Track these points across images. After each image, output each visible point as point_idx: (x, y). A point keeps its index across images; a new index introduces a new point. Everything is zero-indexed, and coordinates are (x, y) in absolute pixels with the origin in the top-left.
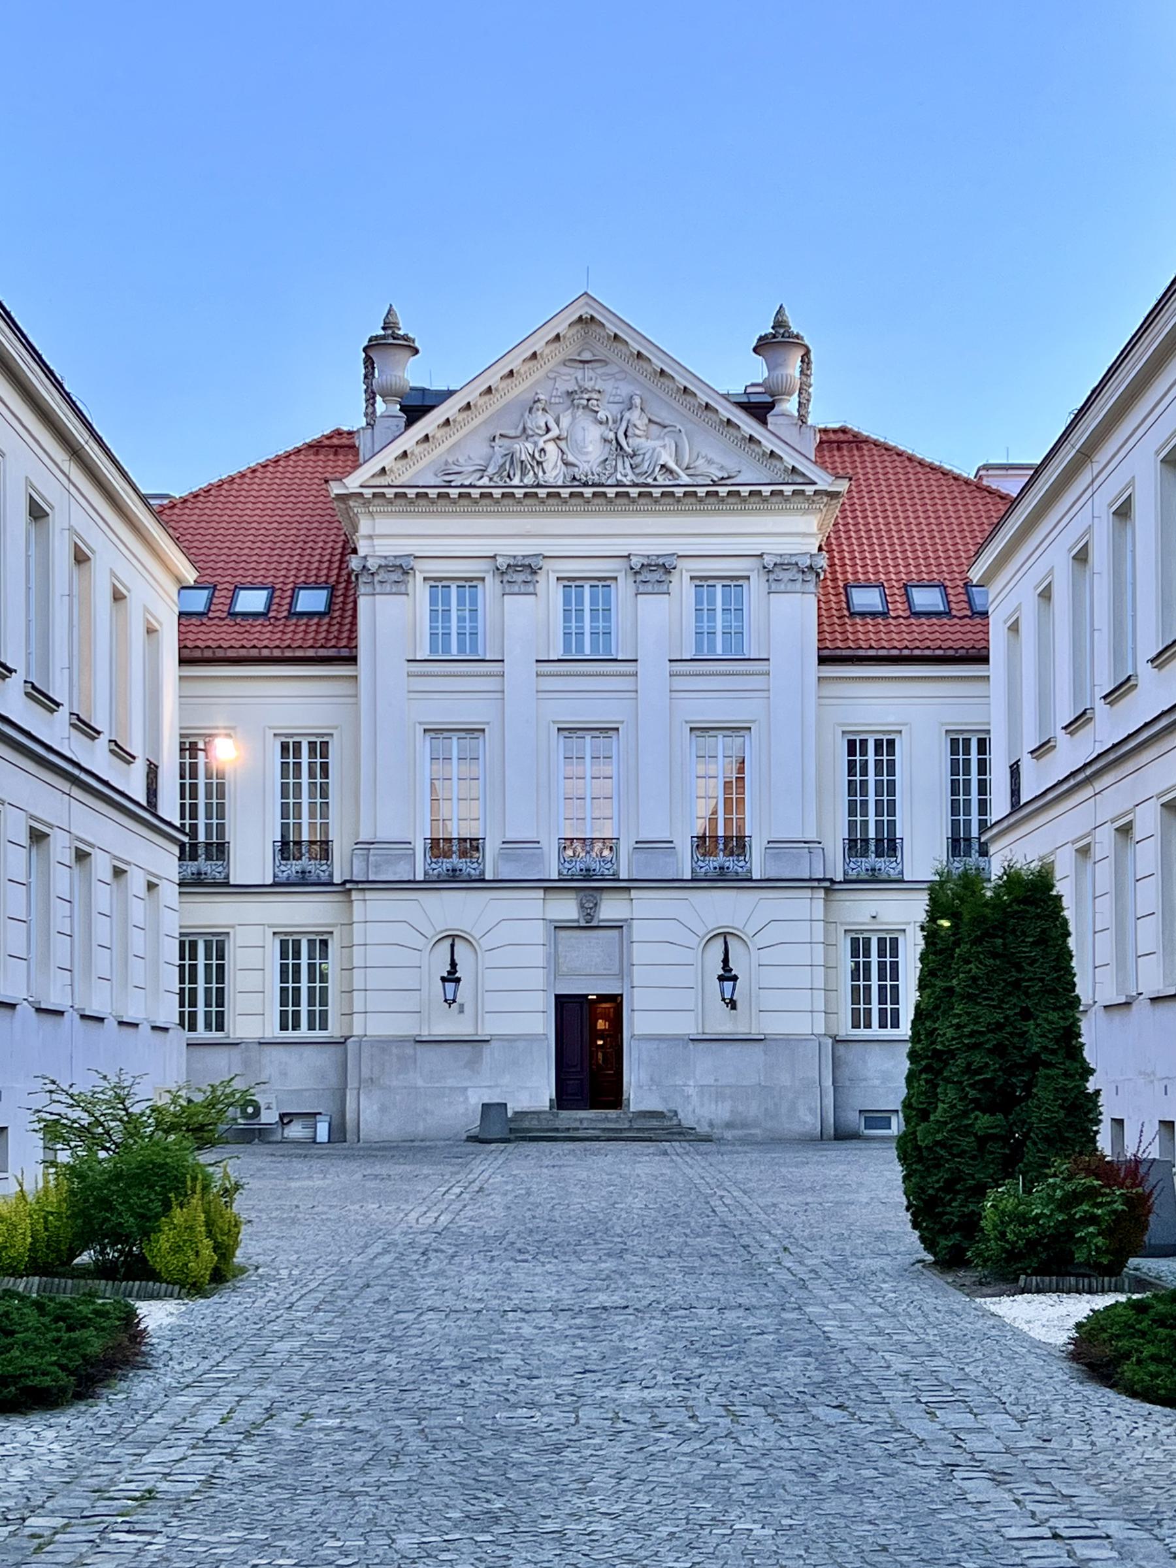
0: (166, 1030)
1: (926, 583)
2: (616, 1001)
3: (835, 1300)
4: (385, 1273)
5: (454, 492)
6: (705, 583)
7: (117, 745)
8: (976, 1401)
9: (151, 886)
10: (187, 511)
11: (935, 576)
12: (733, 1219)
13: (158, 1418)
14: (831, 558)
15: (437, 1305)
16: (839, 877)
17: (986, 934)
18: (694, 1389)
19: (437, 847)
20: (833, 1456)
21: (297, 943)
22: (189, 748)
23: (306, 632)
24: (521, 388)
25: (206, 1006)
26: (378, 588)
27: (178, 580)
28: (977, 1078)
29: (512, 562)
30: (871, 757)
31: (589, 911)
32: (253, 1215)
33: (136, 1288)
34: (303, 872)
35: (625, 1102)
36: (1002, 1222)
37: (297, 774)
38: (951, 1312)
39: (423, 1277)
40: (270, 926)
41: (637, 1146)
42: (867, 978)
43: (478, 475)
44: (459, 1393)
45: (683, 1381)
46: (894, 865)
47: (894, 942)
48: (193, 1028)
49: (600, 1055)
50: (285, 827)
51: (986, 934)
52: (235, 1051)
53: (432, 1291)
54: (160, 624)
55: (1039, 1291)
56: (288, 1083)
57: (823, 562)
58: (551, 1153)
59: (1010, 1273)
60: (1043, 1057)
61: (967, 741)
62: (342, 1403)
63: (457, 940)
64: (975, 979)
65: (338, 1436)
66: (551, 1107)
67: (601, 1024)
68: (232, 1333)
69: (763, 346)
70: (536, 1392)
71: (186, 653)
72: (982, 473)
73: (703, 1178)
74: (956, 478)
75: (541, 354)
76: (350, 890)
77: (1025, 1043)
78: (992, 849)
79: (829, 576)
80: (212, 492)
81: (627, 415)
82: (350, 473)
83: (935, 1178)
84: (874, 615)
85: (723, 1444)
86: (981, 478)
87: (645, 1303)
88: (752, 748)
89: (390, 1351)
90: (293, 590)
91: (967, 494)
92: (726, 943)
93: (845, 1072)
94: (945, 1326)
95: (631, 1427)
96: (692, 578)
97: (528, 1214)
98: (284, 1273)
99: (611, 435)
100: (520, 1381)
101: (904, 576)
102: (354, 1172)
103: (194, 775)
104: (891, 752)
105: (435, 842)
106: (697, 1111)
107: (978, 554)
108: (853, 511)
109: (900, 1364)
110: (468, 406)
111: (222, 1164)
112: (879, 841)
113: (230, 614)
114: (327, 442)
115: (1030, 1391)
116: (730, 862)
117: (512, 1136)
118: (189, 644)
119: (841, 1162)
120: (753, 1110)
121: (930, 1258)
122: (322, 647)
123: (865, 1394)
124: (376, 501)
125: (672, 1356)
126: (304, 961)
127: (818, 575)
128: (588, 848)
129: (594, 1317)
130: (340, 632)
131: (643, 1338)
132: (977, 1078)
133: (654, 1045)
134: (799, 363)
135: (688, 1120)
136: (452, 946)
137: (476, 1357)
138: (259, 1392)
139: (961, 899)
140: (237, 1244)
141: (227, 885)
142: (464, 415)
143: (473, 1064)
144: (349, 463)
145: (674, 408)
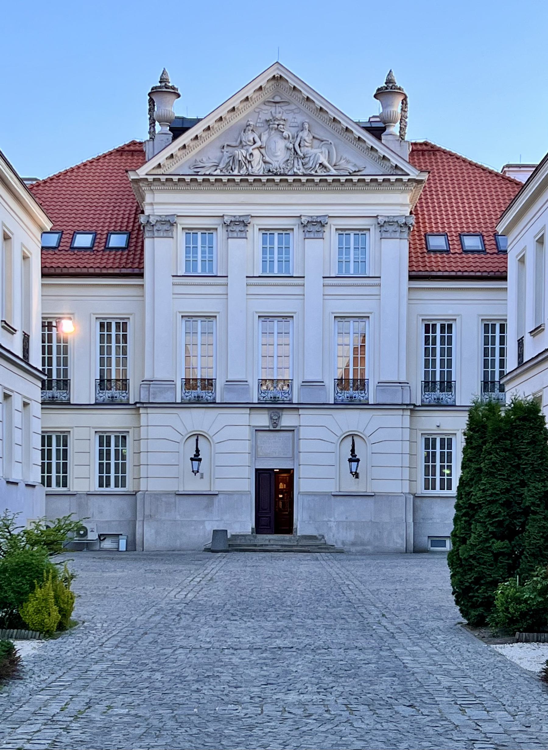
0: (34, 486)
1: (472, 233)
2: (290, 472)
3: (411, 645)
4: (156, 626)
5: (200, 179)
6: (344, 233)
7: (6, 323)
8: (489, 704)
9: (25, 404)
10: (46, 188)
11: (478, 230)
12: (354, 598)
13: (25, 708)
14: (417, 219)
15: (185, 645)
16: (419, 403)
17: (501, 438)
18: (329, 694)
19: (189, 384)
20: (406, 734)
21: (109, 438)
22: (47, 325)
23: (114, 259)
24: (239, 118)
25: (57, 473)
26: (156, 234)
27: (41, 228)
28: (494, 520)
29: (233, 219)
30: (438, 334)
31: (275, 422)
32: (82, 593)
33: (15, 633)
34: (112, 397)
35: (294, 530)
36: (507, 602)
37: (109, 341)
38: (477, 653)
39: (177, 628)
40: (94, 428)
41: (300, 555)
42: (434, 461)
43: (214, 168)
44: (195, 695)
45: (323, 690)
46: (450, 396)
47: (450, 440)
48: (49, 485)
49: (281, 503)
50: (102, 371)
51: (501, 438)
52: (73, 498)
53: (182, 637)
54: (31, 254)
55: (527, 641)
56: (103, 516)
57: (412, 220)
58: (252, 559)
59: (510, 631)
60: (532, 508)
61: (494, 326)
62: (130, 700)
63: (199, 437)
64: (494, 463)
65: (126, 719)
66: (252, 533)
67: (282, 486)
68: (68, 659)
69: (380, 94)
70: (239, 695)
71: (46, 271)
72: (505, 169)
73: (337, 574)
74: (490, 172)
75: (251, 98)
76: (139, 407)
77: (522, 500)
78: (506, 389)
79: (415, 229)
80: (61, 177)
81: (301, 134)
82: (140, 167)
83: (468, 577)
84: (441, 252)
85: (343, 726)
86: (505, 172)
87: (302, 645)
88: (370, 328)
89: (158, 671)
90: (107, 234)
91: (496, 182)
92: (353, 440)
93: (420, 514)
94: (472, 661)
95: (292, 716)
96: (260, 229)
97: (238, 593)
98: (99, 625)
99: (291, 146)
100: (230, 689)
101: (459, 229)
102: (140, 568)
103: (50, 341)
104: (450, 331)
105: (187, 380)
106: (335, 536)
107: (502, 217)
108: (430, 191)
109: (446, 682)
110: (209, 128)
111: (64, 563)
112: (442, 382)
113: (71, 248)
114: (127, 148)
115: (519, 698)
116: (357, 394)
117: (230, 549)
118: (48, 265)
119: (417, 566)
120: (366, 536)
121: (466, 621)
122: (124, 267)
123: (426, 699)
124: (155, 183)
125: (317, 675)
126: (113, 448)
127: (409, 228)
128: (275, 385)
129: (272, 652)
130: (134, 259)
131: (300, 665)
132: (494, 520)
133: (310, 498)
134: (401, 104)
135: (330, 539)
136: (197, 440)
137: (206, 675)
138: (83, 693)
139: (488, 419)
140: (72, 609)
141: (69, 404)
142: (206, 133)
143: (208, 507)
144: (140, 161)
145: (327, 130)
